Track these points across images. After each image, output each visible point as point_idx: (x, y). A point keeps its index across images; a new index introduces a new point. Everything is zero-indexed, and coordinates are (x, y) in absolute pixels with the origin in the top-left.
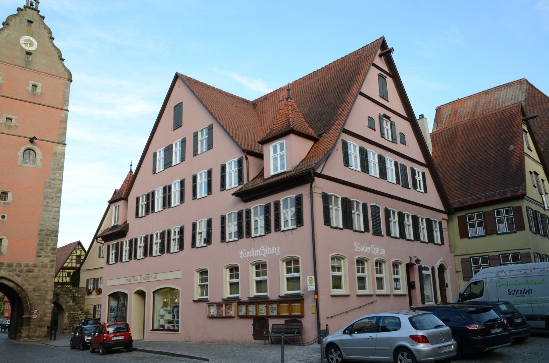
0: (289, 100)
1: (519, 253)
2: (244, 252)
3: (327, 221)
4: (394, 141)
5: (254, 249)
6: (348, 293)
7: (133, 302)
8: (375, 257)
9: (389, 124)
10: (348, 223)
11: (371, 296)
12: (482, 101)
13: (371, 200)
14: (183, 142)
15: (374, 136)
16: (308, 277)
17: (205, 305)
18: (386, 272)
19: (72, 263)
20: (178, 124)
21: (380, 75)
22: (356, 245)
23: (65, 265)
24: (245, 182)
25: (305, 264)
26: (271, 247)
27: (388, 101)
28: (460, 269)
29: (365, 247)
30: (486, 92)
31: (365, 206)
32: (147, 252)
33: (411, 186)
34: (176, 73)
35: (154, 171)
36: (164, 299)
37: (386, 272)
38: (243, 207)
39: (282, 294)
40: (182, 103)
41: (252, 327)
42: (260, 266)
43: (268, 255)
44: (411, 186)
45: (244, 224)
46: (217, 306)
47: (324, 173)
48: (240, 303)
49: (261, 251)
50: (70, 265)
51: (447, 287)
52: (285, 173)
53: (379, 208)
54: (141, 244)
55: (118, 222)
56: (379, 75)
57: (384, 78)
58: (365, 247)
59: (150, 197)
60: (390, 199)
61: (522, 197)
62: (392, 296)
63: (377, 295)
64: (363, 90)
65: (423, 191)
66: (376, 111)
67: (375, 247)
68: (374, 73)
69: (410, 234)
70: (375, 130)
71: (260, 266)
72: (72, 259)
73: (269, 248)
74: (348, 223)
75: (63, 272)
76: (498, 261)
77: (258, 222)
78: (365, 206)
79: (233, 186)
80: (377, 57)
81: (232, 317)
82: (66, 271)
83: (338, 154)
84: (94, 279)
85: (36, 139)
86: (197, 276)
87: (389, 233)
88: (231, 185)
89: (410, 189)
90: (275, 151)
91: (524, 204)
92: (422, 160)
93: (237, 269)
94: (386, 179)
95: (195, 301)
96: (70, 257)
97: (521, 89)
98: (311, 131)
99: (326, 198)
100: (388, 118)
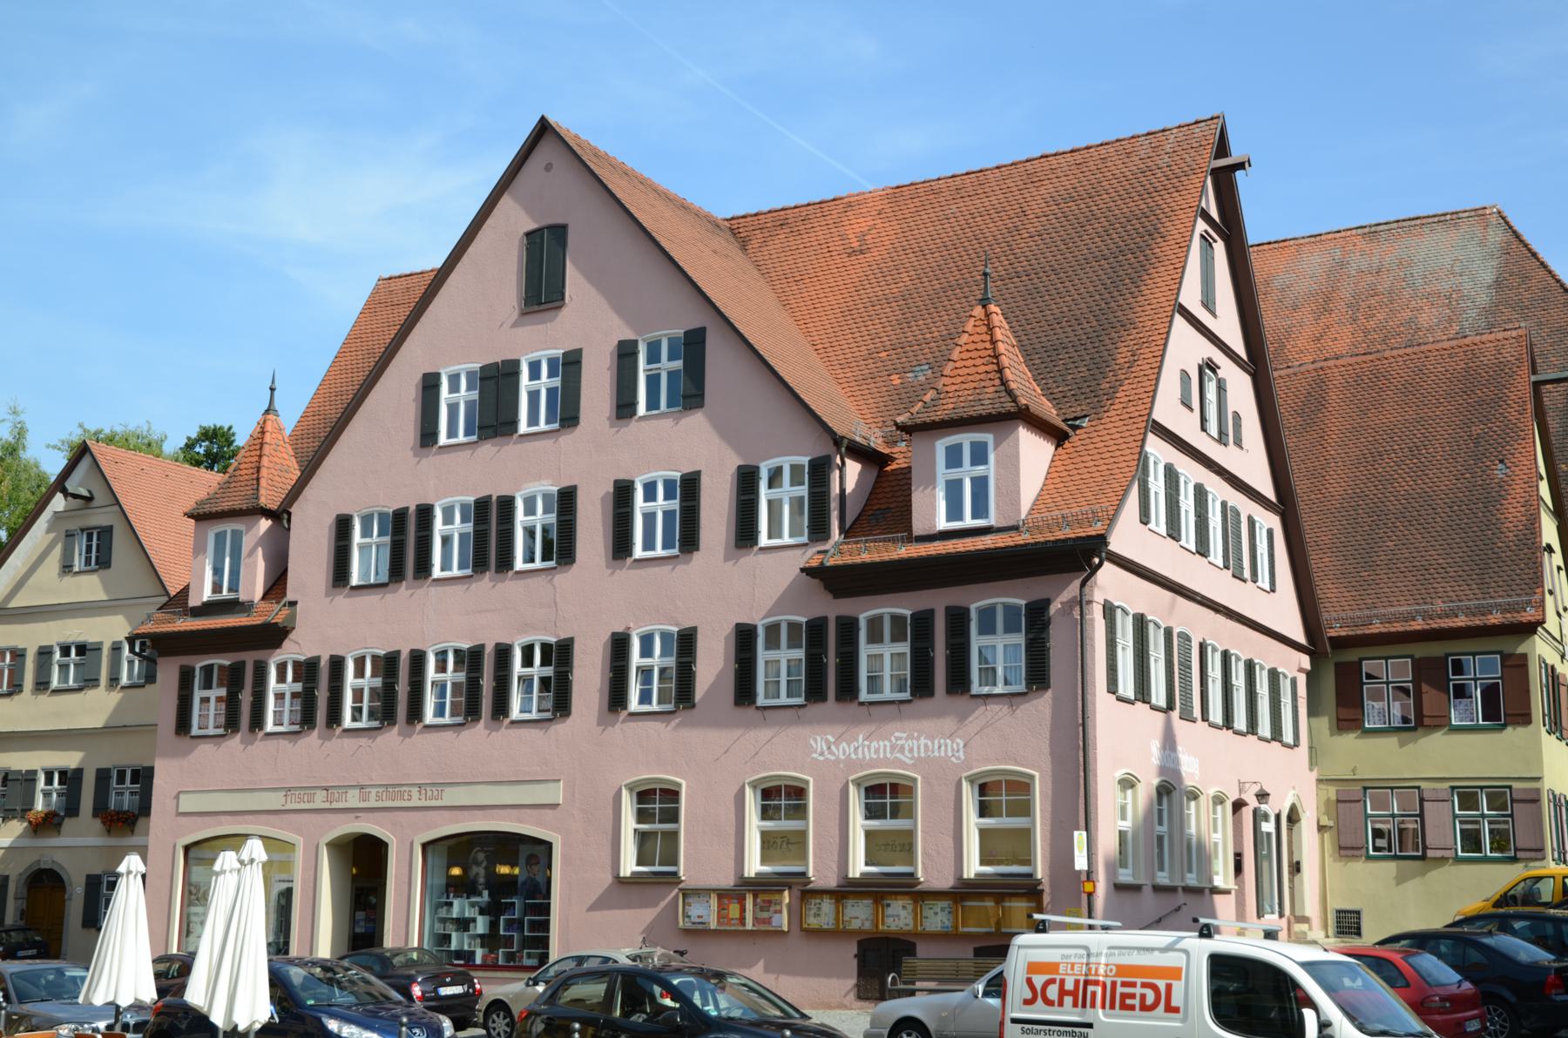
1: (1510, 787)
2: (827, 741)
3: (1112, 686)
12: (1357, 262)
27: (1215, 316)
30: (1371, 232)
33: (1247, 574)
34: (543, 118)
36: (449, 867)
38: (833, 609)
41: (855, 962)
42: (886, 796)
44: (1247, 574)
45: (832, 660)
46: (720, 897)
49: (893, 747)
62: (1147, 890)
65: (1267, 586)
69: (1241, 722)
71: (886, 796)
73: (923, 741)
76: (1447, 805)
77: (882, 660)
81: (779, 933)
87: (1205, 718)
92: (1269, 491)
94: (1178, 540)
97: (1482, 244)
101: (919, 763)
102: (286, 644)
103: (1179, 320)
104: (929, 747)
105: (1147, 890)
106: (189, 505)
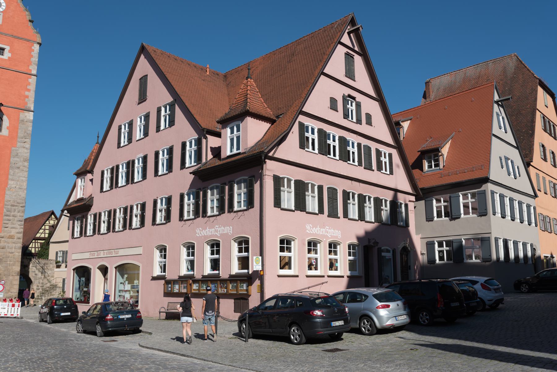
0: (249, 80)
3: (277, 203)
4: (359, 121)
5: (209, 228)
6: (297, 274)
7: (97, 276)
8: (329, 238)
9: (354, 104)
10: (300, 205)
11: (323, 276)
13: (327, 182)
14: (147, 117)
15: (337, 117)
16: (255, 257)
17: (163, 282)
18: (322, 255)
19: (45, 233)
20: (143, 98)
21: (347, 54)
22: (308, 227)
23: (38, 235)
24: (204, 160)
25: (253, 245)
26: (224, 227)
27: (355, 81)
28: (425, 252)
29: (318, 229)
31: (320, 188)
32: (111, 228)
33: (374, 166)
35: (119, 146)
37: (322, 255)
39: (206, 274)
40: (147, 75)
42: (215, 246)
43: (221, 234)
44: (374, 166)
45: (201, 203)
47: (276, 156)
48: (195, 281)
49: (215, 230)
50: (43, 236)
51: (410, 269)
52: (239, 154)
53: (337, 190)
54: (104, 218)
55: (238, 148)
56: (345, 53)
57: (352, 57)
58: (318, 229)
59: (115, 171)
60: (350, 181)
61: (486, 180)
62: (326, 277)
63: (329, 276)
64: (326, 71)
66: (339, 92)
67: (329, 229)
68: (340, 51)
70: (337, 111)
72: (45, 229)
74: (300, 205)
75: (35, 242)
78: (320, 188)
79: (193, 164)
80: (346, 35)
82: (39, 241)
83: (294, 137)
84: (63, 252)
85: (3, 105)
86: (184, 251)
87: (346, 215)
88: (122, 183)
89: (373, 171)
90: (232, 132)
91: (490, 187)
93: (218, 245)
95: (154, 279)
96: (43, 227)
98: (269, 113)
99: (278, 181)
100: (354, 98)
101: (222, 235)
102: (92, 210)
103: (493, 138)
104: (224, 228)
105: (326, 277)
106: (75, 171)
